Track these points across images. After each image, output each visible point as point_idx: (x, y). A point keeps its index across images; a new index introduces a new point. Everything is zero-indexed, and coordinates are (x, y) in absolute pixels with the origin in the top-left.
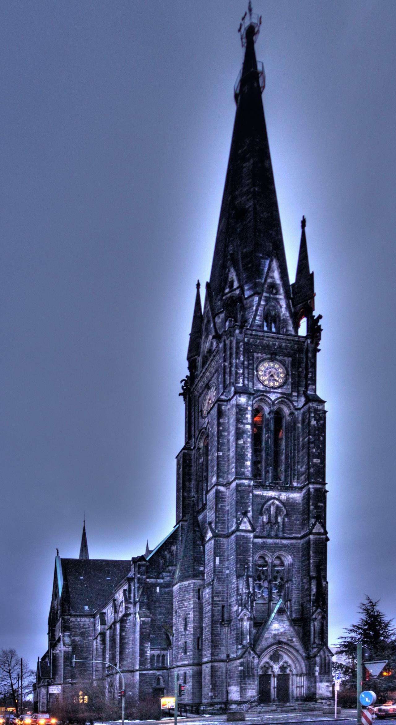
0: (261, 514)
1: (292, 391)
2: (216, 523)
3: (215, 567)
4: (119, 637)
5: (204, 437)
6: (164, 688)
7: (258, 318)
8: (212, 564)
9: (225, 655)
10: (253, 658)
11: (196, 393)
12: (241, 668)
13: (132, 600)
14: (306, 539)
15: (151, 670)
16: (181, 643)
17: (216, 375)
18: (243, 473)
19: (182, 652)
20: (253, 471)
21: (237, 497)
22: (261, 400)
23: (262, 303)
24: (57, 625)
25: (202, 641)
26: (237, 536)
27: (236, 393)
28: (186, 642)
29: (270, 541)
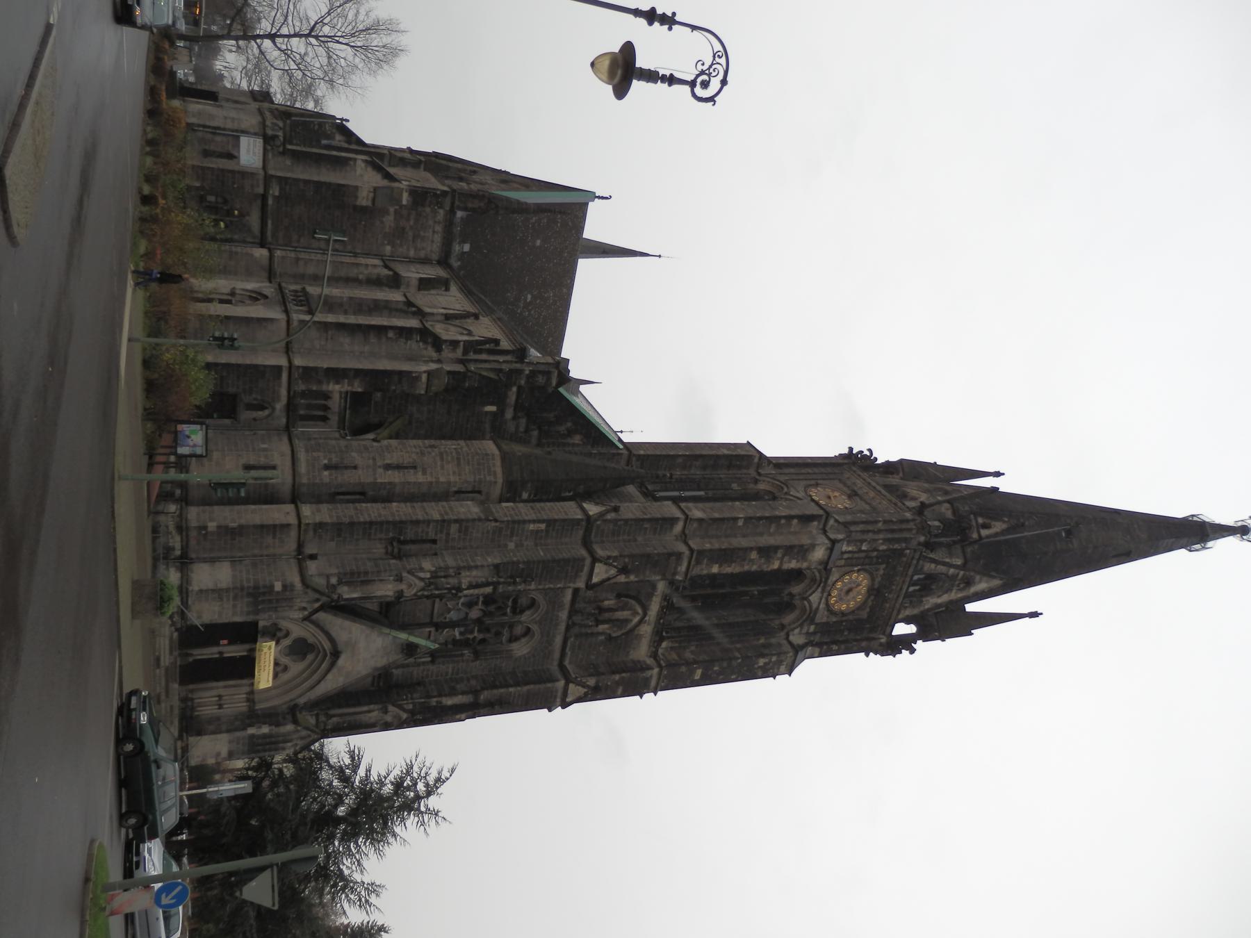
0: (619, 596)
1: (817, 624)
2: (615, 521)
3: (524, 522)
4: (385, 323)
5: (775, 491)
6: (235, 418)
7: (933, 566)
8: (533, 517)
9: (314, 551)
10: (305, 609)
11: (847, 475)
12: (278, 587)
13: (472, 356)
14: (558, 674)
15: (289, 392)
16: (356, 457)
17: (867, 507)
18: (698, 562)
19: (330, 460)
20: (700, 576)
21: (658, 554)
22: (813, 580)
23: (952, 571)
24: (428, 175)
25: (353, 502)
26: (583, 559)
27: (834, 542)
28: (355, 468)
29: (564, 615)
